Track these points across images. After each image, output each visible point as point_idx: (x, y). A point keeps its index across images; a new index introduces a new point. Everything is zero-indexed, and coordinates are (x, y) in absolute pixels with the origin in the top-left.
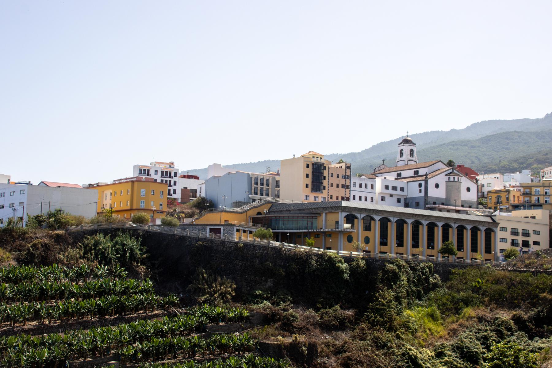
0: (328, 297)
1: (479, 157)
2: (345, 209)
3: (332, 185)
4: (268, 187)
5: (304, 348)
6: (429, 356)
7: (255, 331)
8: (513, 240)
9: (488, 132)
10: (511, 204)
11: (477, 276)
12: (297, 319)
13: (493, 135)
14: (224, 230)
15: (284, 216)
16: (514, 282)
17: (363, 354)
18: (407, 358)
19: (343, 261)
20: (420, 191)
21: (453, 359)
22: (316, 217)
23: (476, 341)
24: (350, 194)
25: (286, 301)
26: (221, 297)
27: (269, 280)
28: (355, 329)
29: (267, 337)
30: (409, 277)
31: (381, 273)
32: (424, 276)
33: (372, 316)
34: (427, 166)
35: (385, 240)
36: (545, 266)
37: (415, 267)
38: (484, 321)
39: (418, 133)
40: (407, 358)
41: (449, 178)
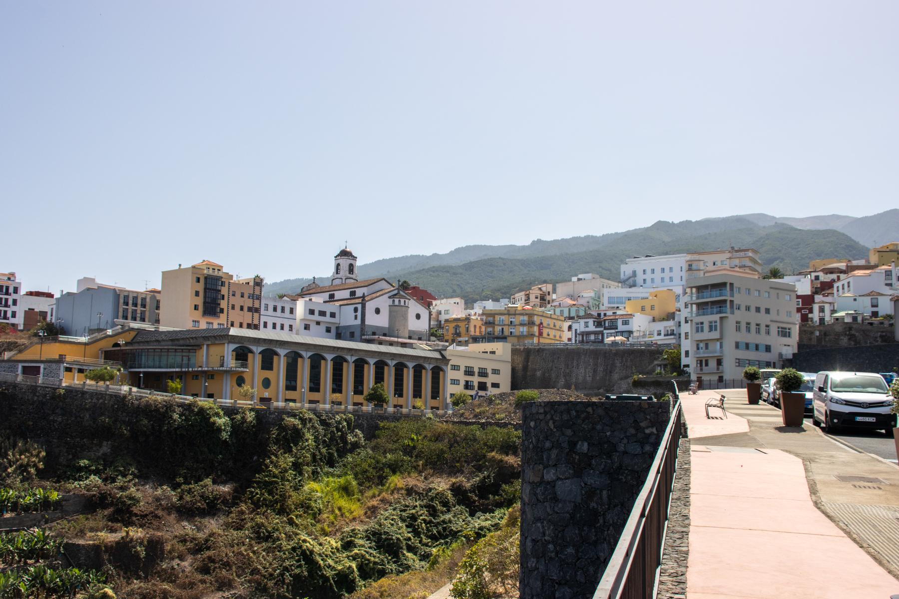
0: (195, 466)
1: (462, 285)
2: (234, 339)
3: (233, 307)
4: (127, 307)
5: (139, 549)
6: (332, 548)
7: (62, 525)
8: (467, 382)
9: (472, 259)
10: (471, 336)
11: (412, 432)
12: (138, 502)
13: (476, 262)
14: (45, 369)
15: (148, 349)
16: (458, 439)
17: (233, 552)
18: (299, 553)
19: (222, 413)
20: (356, 318)
21: (365, 551)
22: (194, 351)
23: (399, 523)
24: (259, 319)
25: (127, 475)
26: (19, 471)
27: (105, 443)
28: (231, 512)
29: (81, 533)
30: (318, 434)
31: (276, 430)
32: (339, 433)
33: (257, 494)
34: (367, 284)
35: (293, 383)
36: (497, 416)
37: (328, 421)
38: (414, 494)
39: (397, 257)
40: (299, 553)
41: (394, 301)
